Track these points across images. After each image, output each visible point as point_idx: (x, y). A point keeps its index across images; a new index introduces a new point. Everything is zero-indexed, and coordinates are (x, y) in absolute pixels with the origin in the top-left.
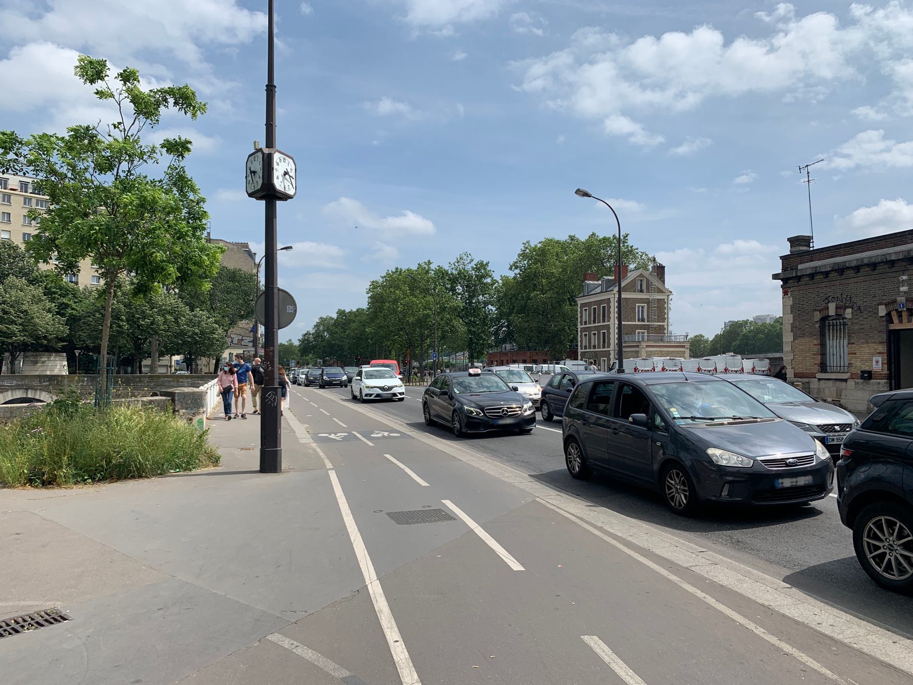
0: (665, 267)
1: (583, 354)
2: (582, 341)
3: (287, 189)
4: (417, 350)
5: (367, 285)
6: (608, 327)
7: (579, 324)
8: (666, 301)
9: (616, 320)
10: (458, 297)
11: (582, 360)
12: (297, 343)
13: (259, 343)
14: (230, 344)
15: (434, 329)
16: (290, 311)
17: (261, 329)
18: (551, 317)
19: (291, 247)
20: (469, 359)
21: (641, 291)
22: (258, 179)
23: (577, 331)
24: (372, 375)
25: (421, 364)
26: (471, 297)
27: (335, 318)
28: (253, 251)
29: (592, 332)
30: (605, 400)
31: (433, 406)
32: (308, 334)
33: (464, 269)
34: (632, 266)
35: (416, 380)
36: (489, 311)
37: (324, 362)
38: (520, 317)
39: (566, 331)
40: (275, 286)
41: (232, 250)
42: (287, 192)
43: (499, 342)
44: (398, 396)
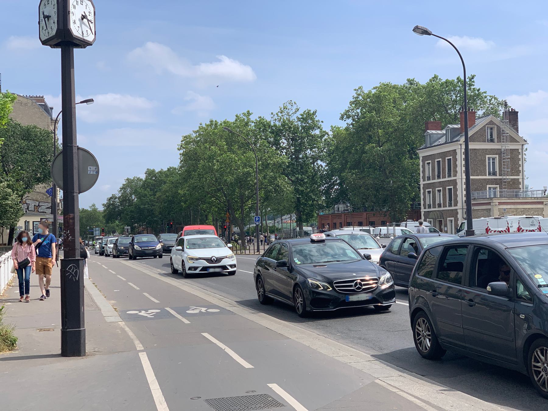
0: (518, 112)
1: (427, 214)
2: (425, 198)
3: (85, 35)
4: (237, 214)
5: (178, 140)
6: (454, 183)
7: (421, 180)
8: (520, 151)
9: (464, 175)
10: (283, 152)
11: (426, 221)
12: (101, 208)
13: (58, 209)
14: (26, 211)
15: (256, 189)
16: (92, 173)
17: (60, 194)
18: (390, 173)
19: (92, 100)
20: (296, 222)
21: (492, 141)
22: (53, 25)
23: (419, 188)
24: (195, 244)
25: (241, 229)
26: (297, 152)
27: (144, 179)
28: (49, 105)
29: (437, 189)
30: (458, 267)
31: (268, 280)
32: (113, 197)
33: (289, 121)
34: (480, 113)
35: (236, 248)
36: (318, 168)
37: (133, 229)
38: (353, 173)
39: (406, 189)
40: (74, 145)
41: (26, 104)
42: (85, 38)
43: (331, 203)
44: (229, 269)
